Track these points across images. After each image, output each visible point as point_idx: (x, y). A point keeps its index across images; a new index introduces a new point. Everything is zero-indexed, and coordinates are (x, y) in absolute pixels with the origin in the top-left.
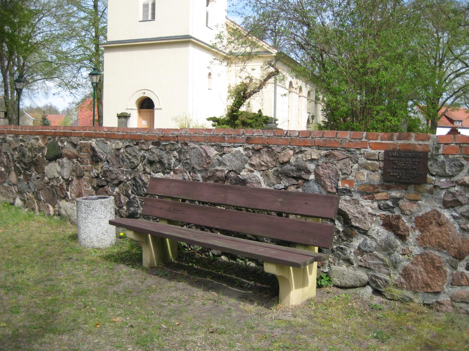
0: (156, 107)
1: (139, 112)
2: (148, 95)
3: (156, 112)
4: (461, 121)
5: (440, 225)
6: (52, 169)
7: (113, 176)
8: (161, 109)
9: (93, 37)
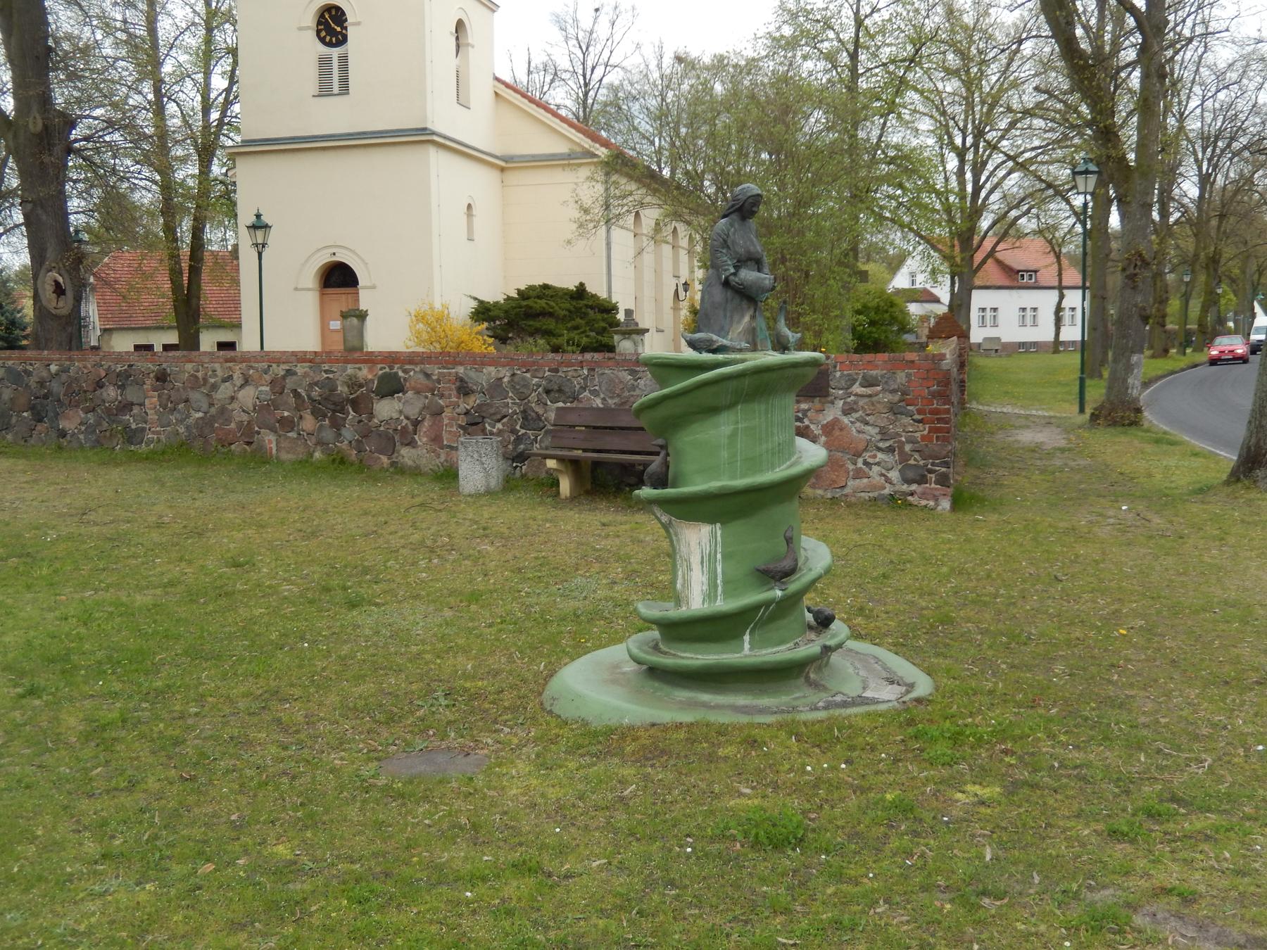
0: (362, 281)
1: (322, 295)
2: (341, 258)
3: (362, 293)
4: (1036, 272)
5: (841, 430)
6: (386, 409)
7: (492, 411)
8: (374, 287)
9: (149, 102)
